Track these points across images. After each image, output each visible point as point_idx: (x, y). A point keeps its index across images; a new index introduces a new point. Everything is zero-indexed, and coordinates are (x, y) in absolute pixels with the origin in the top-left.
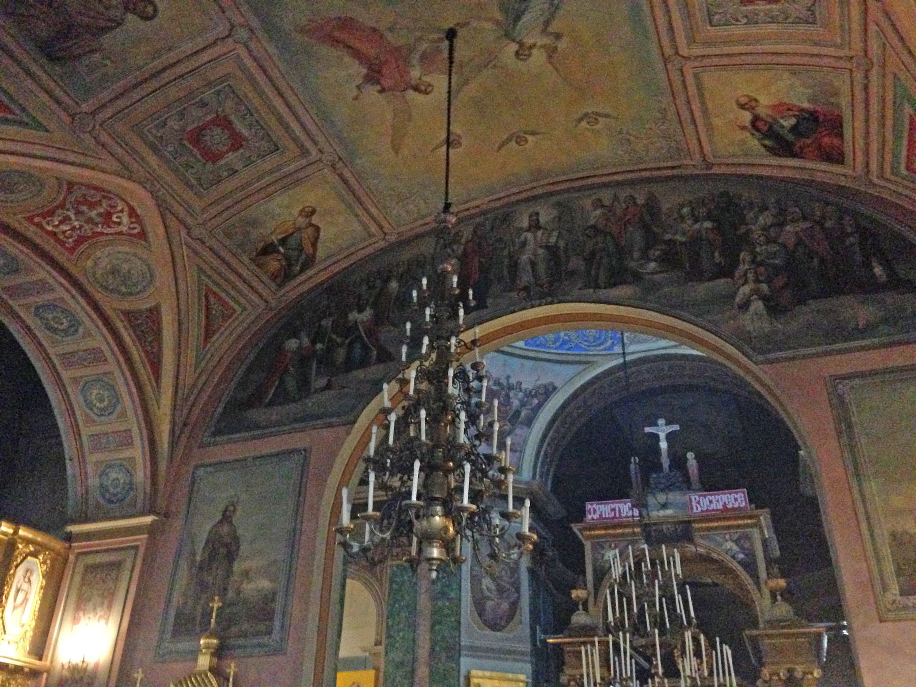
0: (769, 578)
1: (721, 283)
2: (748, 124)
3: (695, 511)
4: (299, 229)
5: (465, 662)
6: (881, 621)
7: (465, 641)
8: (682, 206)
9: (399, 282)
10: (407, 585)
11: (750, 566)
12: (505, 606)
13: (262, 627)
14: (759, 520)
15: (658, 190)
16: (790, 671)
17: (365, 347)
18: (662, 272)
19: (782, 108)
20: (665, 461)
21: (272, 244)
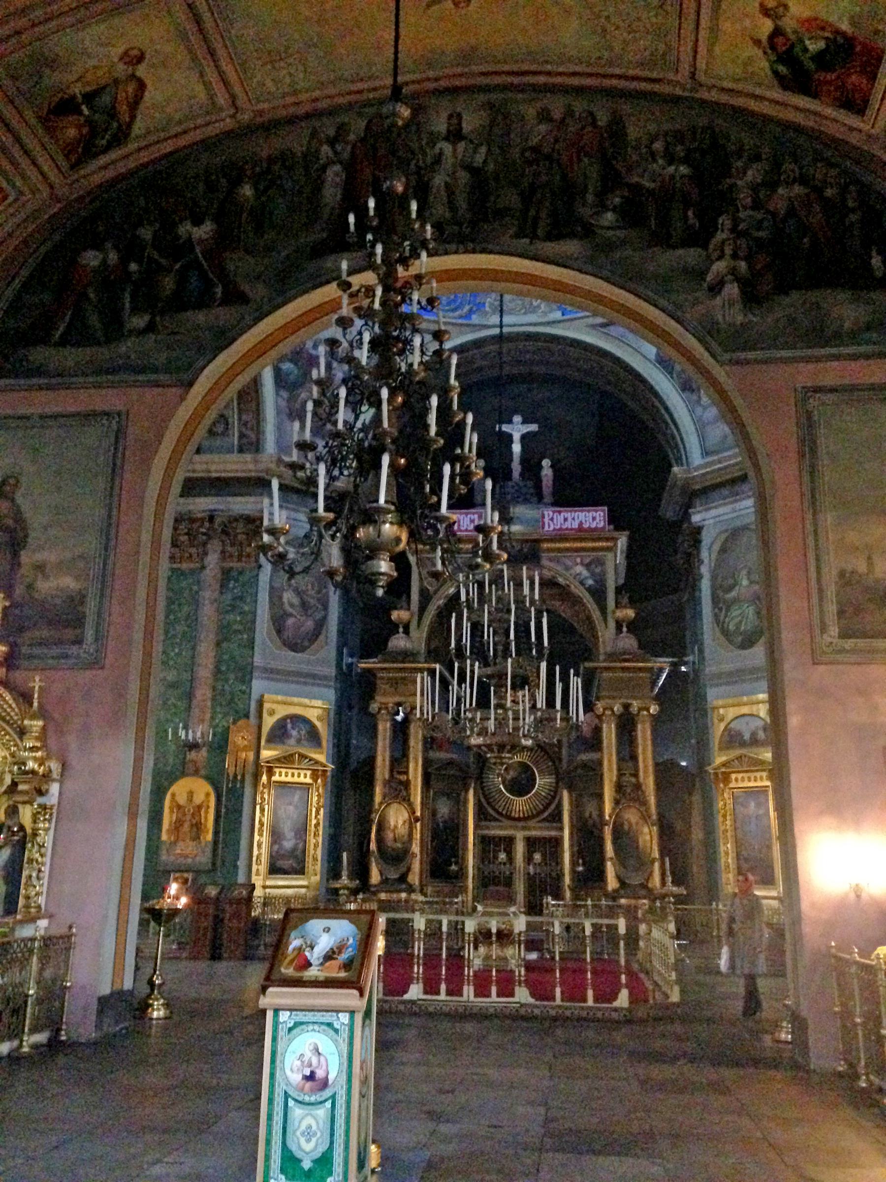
0: (617, 607)
1: (691, 256)
2: (764, 38)
3: (546, 528)
4: (116, 81)
5: (258, 686)
6: (814, 664)
7: (258, 660)
8: (653, 139)
9: (255, 187)
10: (186, 594)
11: (598, 593)
12: (310, 624)
13: (69, 634)
14: (616, 545)
15: (626, 108)
16: (626, 707)
17: (203, 276)
18: (619, 228)
19: (815, 24)
20: (516, 467)
21: (74, 97)
